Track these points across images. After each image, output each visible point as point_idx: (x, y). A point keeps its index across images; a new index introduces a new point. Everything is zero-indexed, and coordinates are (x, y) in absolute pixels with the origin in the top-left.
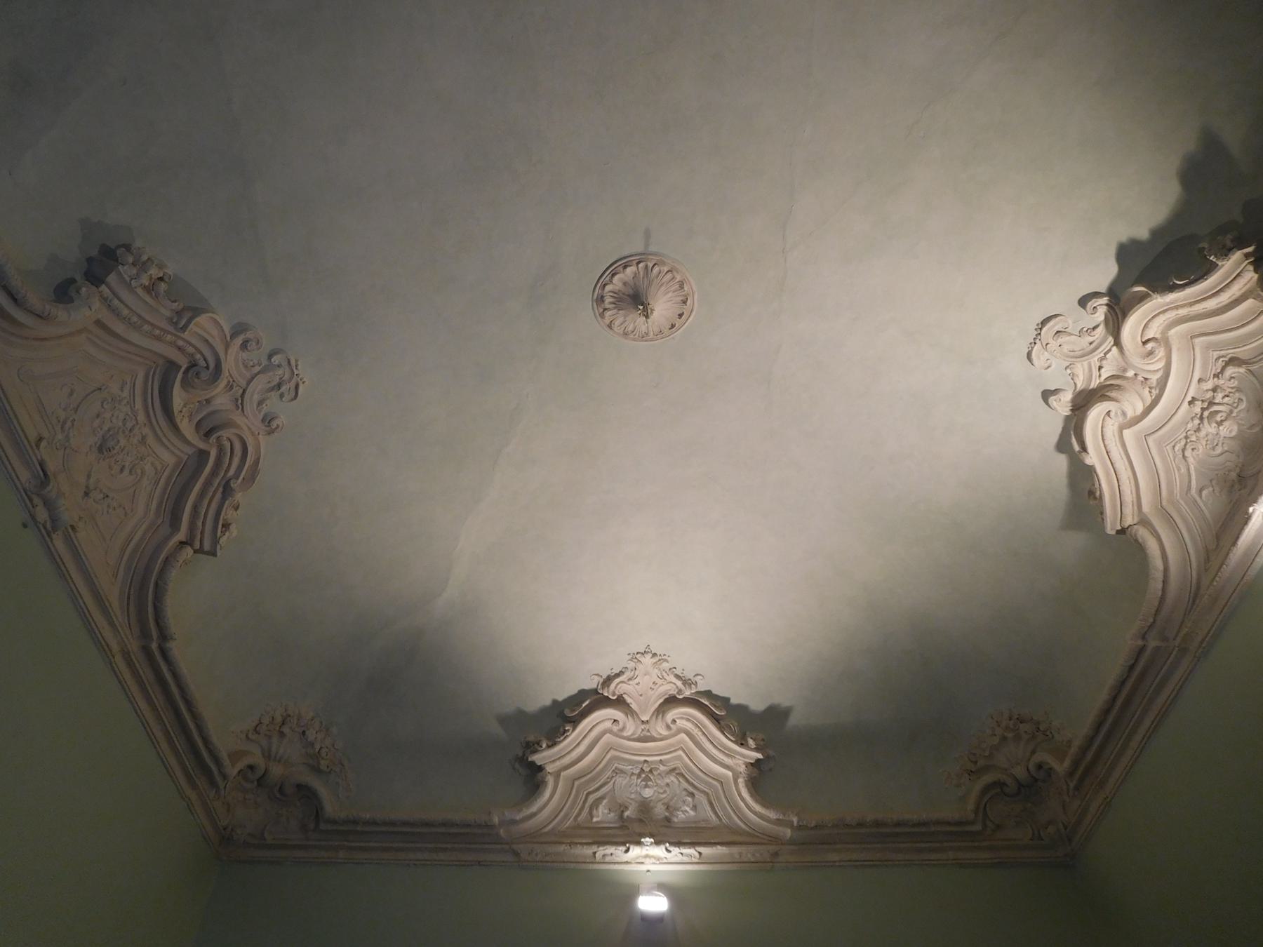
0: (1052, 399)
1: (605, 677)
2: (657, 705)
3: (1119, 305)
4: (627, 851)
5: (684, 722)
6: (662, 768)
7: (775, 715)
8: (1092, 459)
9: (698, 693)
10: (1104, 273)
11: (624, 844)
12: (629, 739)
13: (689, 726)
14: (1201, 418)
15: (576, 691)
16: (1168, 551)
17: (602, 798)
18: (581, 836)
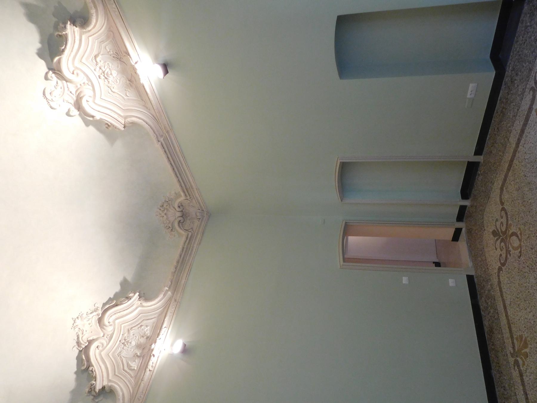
0: (71, 113)
1: (76, 344)
2: (99, 327)
3: (55, 70)
4: (154, 356)
5: (111, 318)
6: (126, 335)
7: (124, 284)
8: (98, 116)
9: (102, 308)
10: (42, 66)
11: (150, 356)
12: (108, 344)
13: (114, 317)
14: (106, 78)
15: (76, 361)
16: (138, 116)
17: (128, 364)
18: (140, 376)
